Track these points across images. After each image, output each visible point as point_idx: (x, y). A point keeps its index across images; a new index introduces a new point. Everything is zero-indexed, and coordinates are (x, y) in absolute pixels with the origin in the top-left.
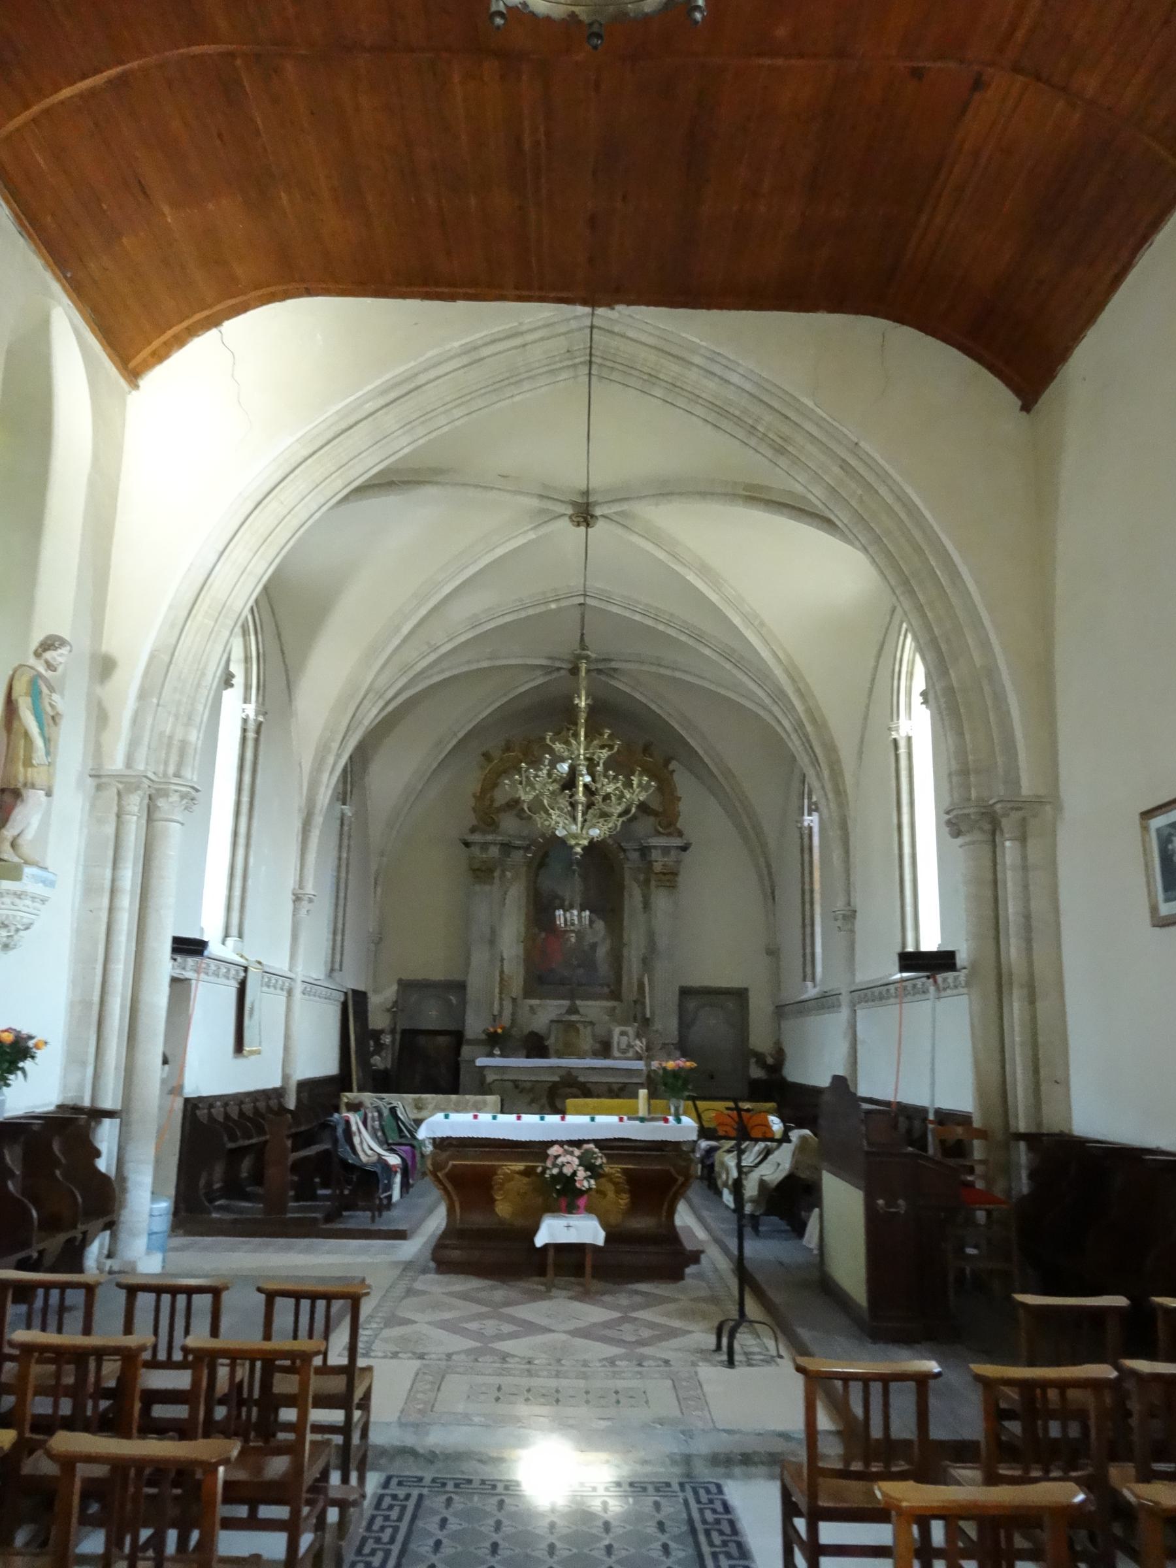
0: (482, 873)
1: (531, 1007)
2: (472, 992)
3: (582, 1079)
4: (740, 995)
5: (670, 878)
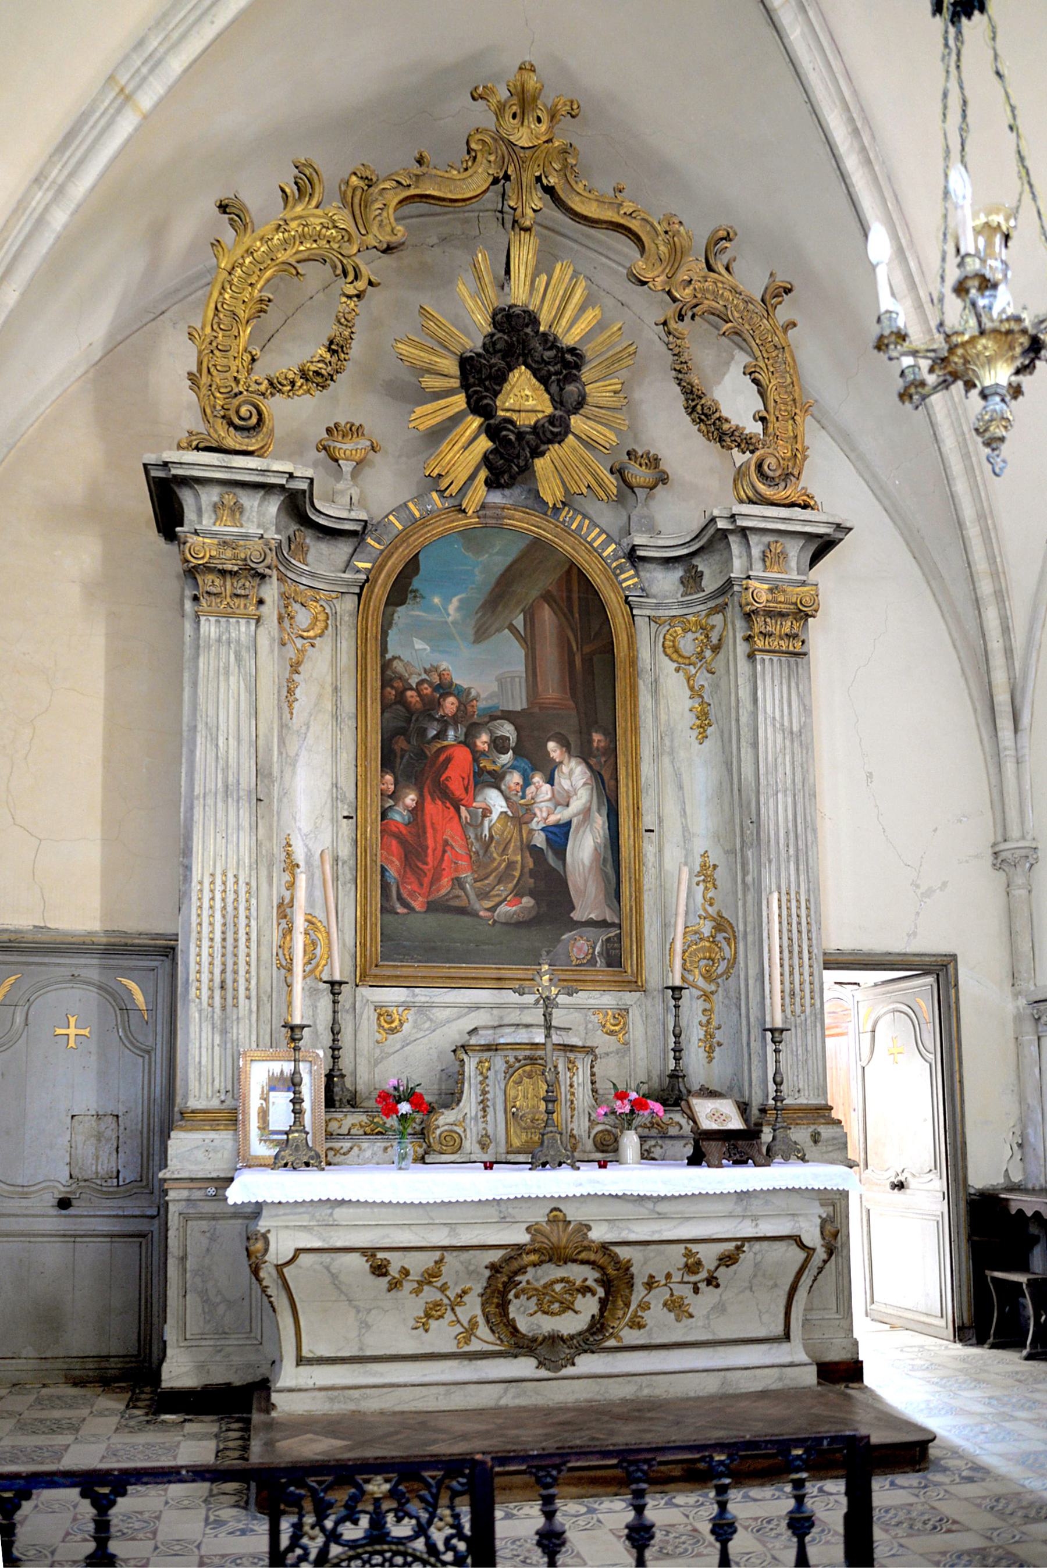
1: (383, 1013)
2: (199, 962)
3: (599, 1234)
4: (166, 1166)
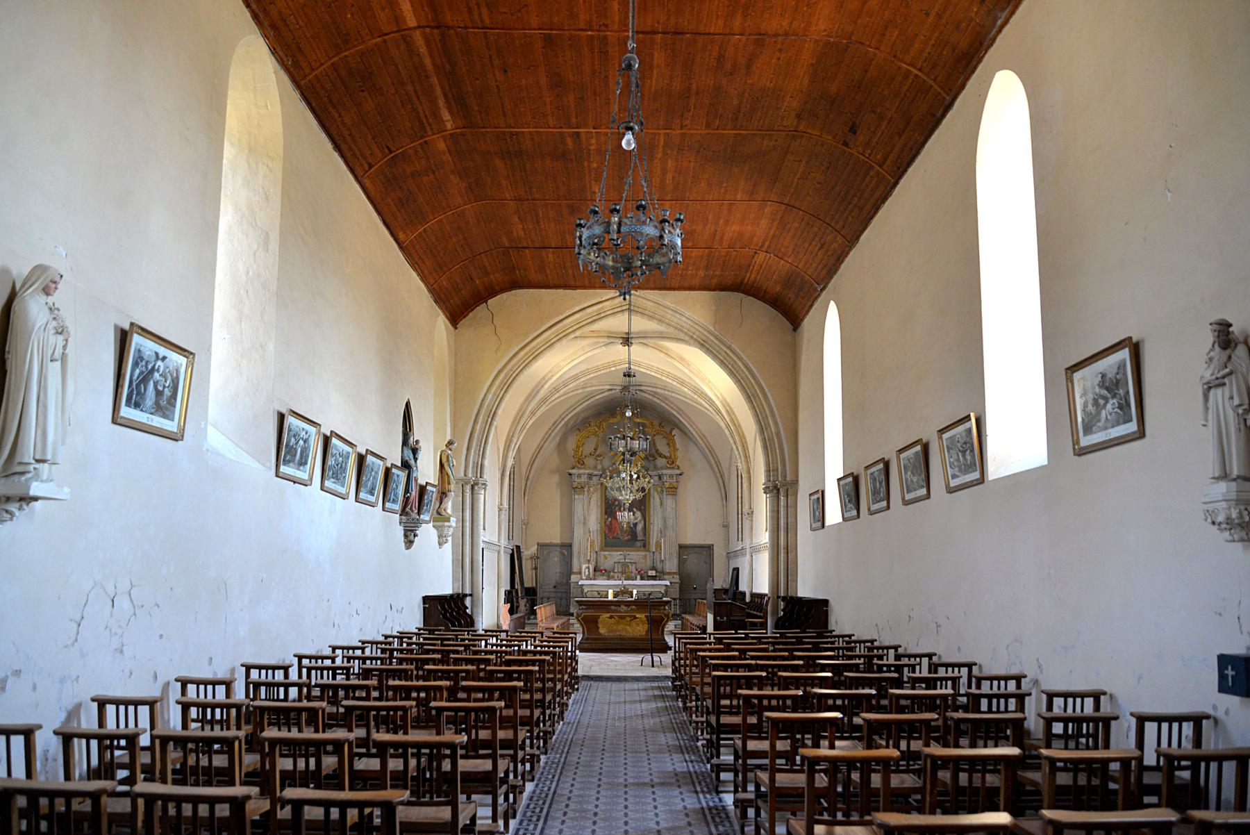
0: (132, 324)
2: (575, 549)
4: (710, 548)
5: (673, 491)
